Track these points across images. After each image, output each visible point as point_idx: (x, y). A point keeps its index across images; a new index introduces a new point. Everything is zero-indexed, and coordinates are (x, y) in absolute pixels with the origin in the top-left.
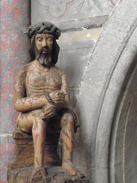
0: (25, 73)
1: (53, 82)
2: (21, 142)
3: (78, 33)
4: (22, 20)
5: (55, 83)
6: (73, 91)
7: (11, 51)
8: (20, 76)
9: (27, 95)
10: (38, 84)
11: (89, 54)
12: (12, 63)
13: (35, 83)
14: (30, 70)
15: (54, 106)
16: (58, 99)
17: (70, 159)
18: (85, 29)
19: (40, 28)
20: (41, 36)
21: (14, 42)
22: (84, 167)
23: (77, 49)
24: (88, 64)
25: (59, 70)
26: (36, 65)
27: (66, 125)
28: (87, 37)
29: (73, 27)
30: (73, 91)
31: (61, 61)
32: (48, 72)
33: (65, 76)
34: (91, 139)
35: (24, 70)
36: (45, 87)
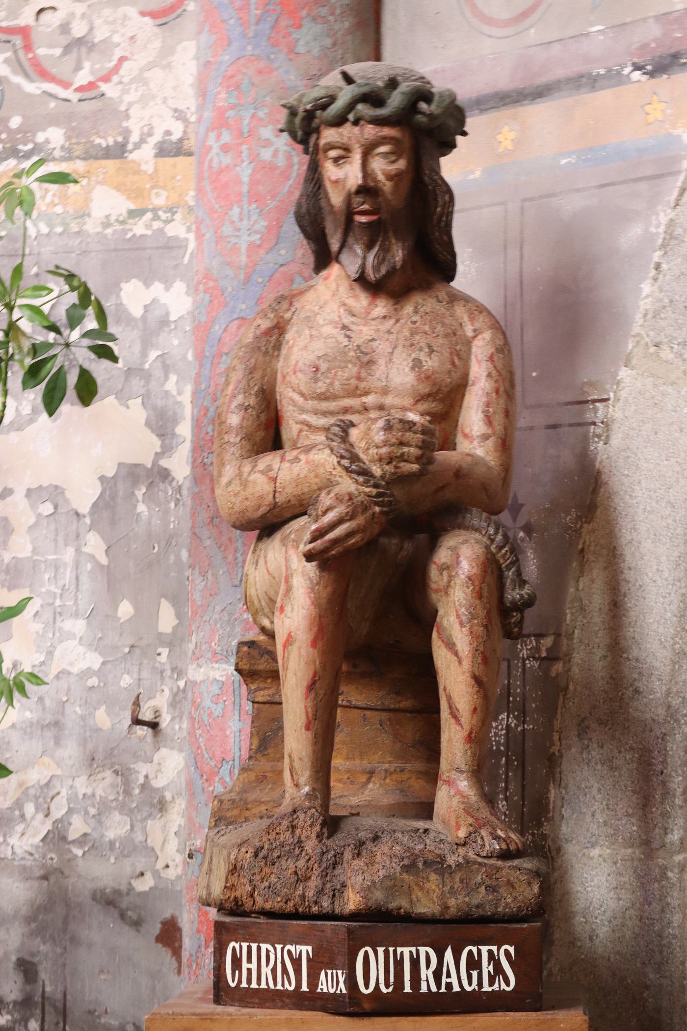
0: (279, 329)
1: (407, 370)
2: (270, 692)
3: (605, 97)
4: (316, 51)
5: (419, 379)
6: (579, 425)
7: (254, 217)
8: (246, 346)
9: (287, 444)
10: (332, 384)
11: (657, 215)
12: (260, 280)
13: (316, 380)
14: (302, 315)
15: (367, 490)
16: (384, 450)
17: (463, 767)
18: (637, 75)
19: (332, 99)
20: (341, 135)
21: (272, 167)
22: (630, 851)
23: (603, 186)
24: (658, 267)
25: (460, 311)
26: (333, 286)
27: (447, 594)
28: (651, 118)
29: (583, 69)
30: (579, 425)
31: (522, 258)
32: (392, 321)
33: (493, 340)
34: (668, 693)
35: (272, 316)
36: (370, 400)
